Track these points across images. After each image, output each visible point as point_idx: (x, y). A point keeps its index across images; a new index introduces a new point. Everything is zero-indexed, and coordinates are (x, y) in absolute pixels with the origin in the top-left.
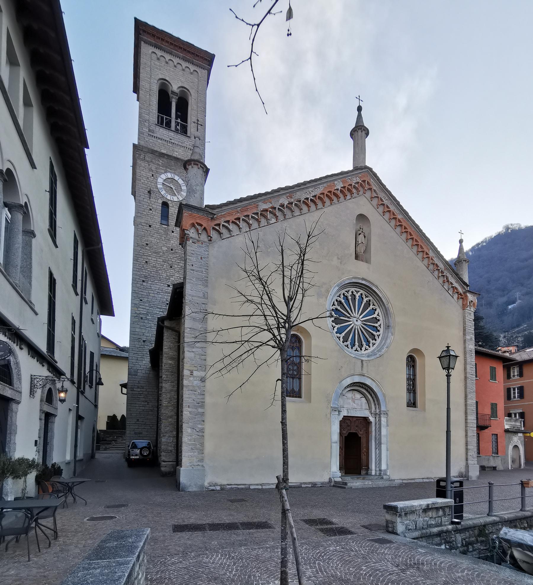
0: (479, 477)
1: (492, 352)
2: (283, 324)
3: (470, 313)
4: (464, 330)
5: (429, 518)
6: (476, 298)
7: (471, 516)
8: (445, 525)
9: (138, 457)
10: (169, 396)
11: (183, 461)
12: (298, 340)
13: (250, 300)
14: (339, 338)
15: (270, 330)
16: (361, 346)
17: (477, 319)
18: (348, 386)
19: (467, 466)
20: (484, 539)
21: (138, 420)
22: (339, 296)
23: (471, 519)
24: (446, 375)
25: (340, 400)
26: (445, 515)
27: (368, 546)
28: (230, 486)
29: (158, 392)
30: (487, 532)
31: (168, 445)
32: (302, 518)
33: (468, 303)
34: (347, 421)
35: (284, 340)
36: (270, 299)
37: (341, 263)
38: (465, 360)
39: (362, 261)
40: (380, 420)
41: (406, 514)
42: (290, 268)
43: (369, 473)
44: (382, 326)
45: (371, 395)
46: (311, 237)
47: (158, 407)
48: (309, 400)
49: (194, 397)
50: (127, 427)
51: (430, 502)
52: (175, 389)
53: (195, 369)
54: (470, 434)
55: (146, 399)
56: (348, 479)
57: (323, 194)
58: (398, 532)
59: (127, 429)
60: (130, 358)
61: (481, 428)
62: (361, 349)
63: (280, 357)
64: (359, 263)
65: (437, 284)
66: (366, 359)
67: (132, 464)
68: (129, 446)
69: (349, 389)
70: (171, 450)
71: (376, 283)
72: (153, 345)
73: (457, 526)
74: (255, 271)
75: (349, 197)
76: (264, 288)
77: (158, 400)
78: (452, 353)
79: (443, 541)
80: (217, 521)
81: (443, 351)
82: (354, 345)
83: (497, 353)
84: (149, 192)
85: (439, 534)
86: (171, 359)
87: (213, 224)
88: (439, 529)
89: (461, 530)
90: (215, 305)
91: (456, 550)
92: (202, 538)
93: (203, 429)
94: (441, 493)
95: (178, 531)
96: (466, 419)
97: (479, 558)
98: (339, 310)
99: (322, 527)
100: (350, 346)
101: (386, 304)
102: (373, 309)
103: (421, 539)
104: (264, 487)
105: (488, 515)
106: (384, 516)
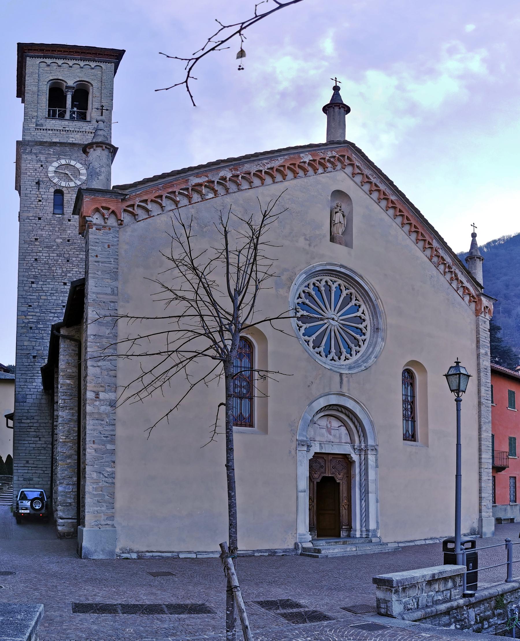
0: (494, 534)
1: (510, 371)
2: (227, 326)
3: (485, 322)
4: (478, 342)
5: (436, 593)
6: (492, 304)
7: (486, 585)
8: (456, 600)
9: (28, 511)
10: (67, 429)
11: (86, 518)
12: (248, 344)
13: (180, 297)
14: (308, 342)
15: (208, 334)
16: (339, 354)
17: (494, 329)
18: (321, 410)
19: (481, 520)
20: (501, 611)
21: (27, 462)
22: (308, 286)
23: (487, 588)
24: (456, 400)
25: (310, 429)
26: (455, 587)
27: (352, 635)
28: (151, 554)
29: (53, 423)
30: (505, 602)
31: (66, 497)
32: (256, 600)
33: (483, 308)
34: (320, 460)
35: (229, 348)
36: (209, 294)
37: (310, 245)
38: (479, 380)
39: (340, 244)
40: (366, 459)
41: (404, 589)
42: (238, 253)
43: (352, 535)
44: (369, 328)
45: (354, 423)
46: (268, 216)
47: (53, 443)
48: (265, 430)
49: (100, 428)
50: (15, 471)
51: (436, 572)
52: (75, 418)
53: (101, 389)
54: (484, 478)
55: (38, 433)
56: (322, 544)
57: (284, 166)
58: (394, 614)
59: (14, 474)
60: (17, 380)
61: (497, 469)
62: (339, 359)
63: (223, 371)
64: (336, 247)
65: (444, 280)
66: (347, 372)
67: (22, 520)
68: (17, 497)
69: (322, 414)
70: (70, 503)
71: (360, 272)
72: (46, 361)
73: (471, 599)
74: (187, 259)
75: (320, 170)
76: (201, 280)
77: (53, 434)
78: (462, 371)
79: (453, 620)
80: (133, 602)
81: (451, 368)
82: (330, 353)
83: (516, 373)
84: (38, 183)
85: (447, 612)
86: (70, 377)
87: (124, 205)
88: (448, 605)
89: (475, 603)
90: (128, 302)
91: (469, 628)
92: (112, 623)
93: (113, 473)
94: (450, 559)
95: (79, 612)
96: (480, 458)
97: (496, 634)
98: (307, 305)
99: (285, 611)
100: (323, 354)
101: (373, 299)
102: (356, 305)
103: (424, 621)
104: (199, 556)
105: (506, 581)
106: (374, 594)
